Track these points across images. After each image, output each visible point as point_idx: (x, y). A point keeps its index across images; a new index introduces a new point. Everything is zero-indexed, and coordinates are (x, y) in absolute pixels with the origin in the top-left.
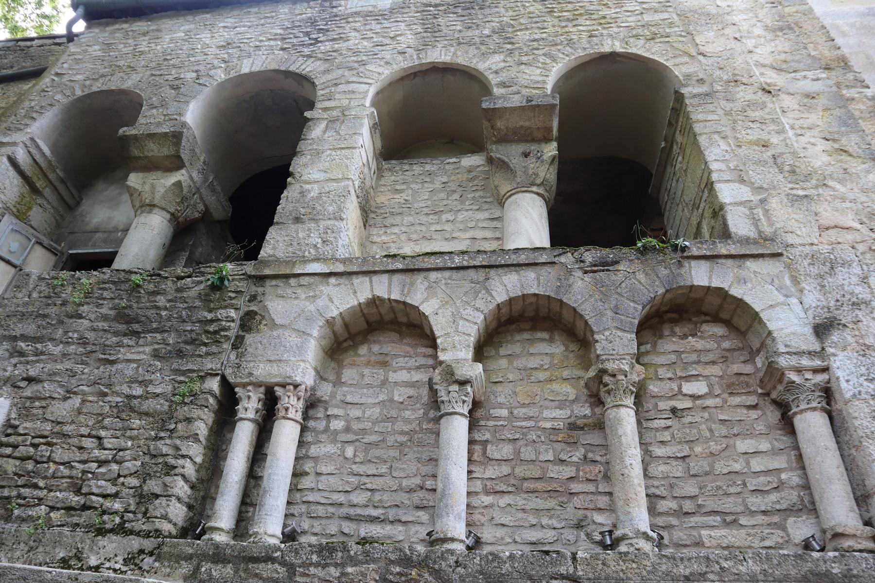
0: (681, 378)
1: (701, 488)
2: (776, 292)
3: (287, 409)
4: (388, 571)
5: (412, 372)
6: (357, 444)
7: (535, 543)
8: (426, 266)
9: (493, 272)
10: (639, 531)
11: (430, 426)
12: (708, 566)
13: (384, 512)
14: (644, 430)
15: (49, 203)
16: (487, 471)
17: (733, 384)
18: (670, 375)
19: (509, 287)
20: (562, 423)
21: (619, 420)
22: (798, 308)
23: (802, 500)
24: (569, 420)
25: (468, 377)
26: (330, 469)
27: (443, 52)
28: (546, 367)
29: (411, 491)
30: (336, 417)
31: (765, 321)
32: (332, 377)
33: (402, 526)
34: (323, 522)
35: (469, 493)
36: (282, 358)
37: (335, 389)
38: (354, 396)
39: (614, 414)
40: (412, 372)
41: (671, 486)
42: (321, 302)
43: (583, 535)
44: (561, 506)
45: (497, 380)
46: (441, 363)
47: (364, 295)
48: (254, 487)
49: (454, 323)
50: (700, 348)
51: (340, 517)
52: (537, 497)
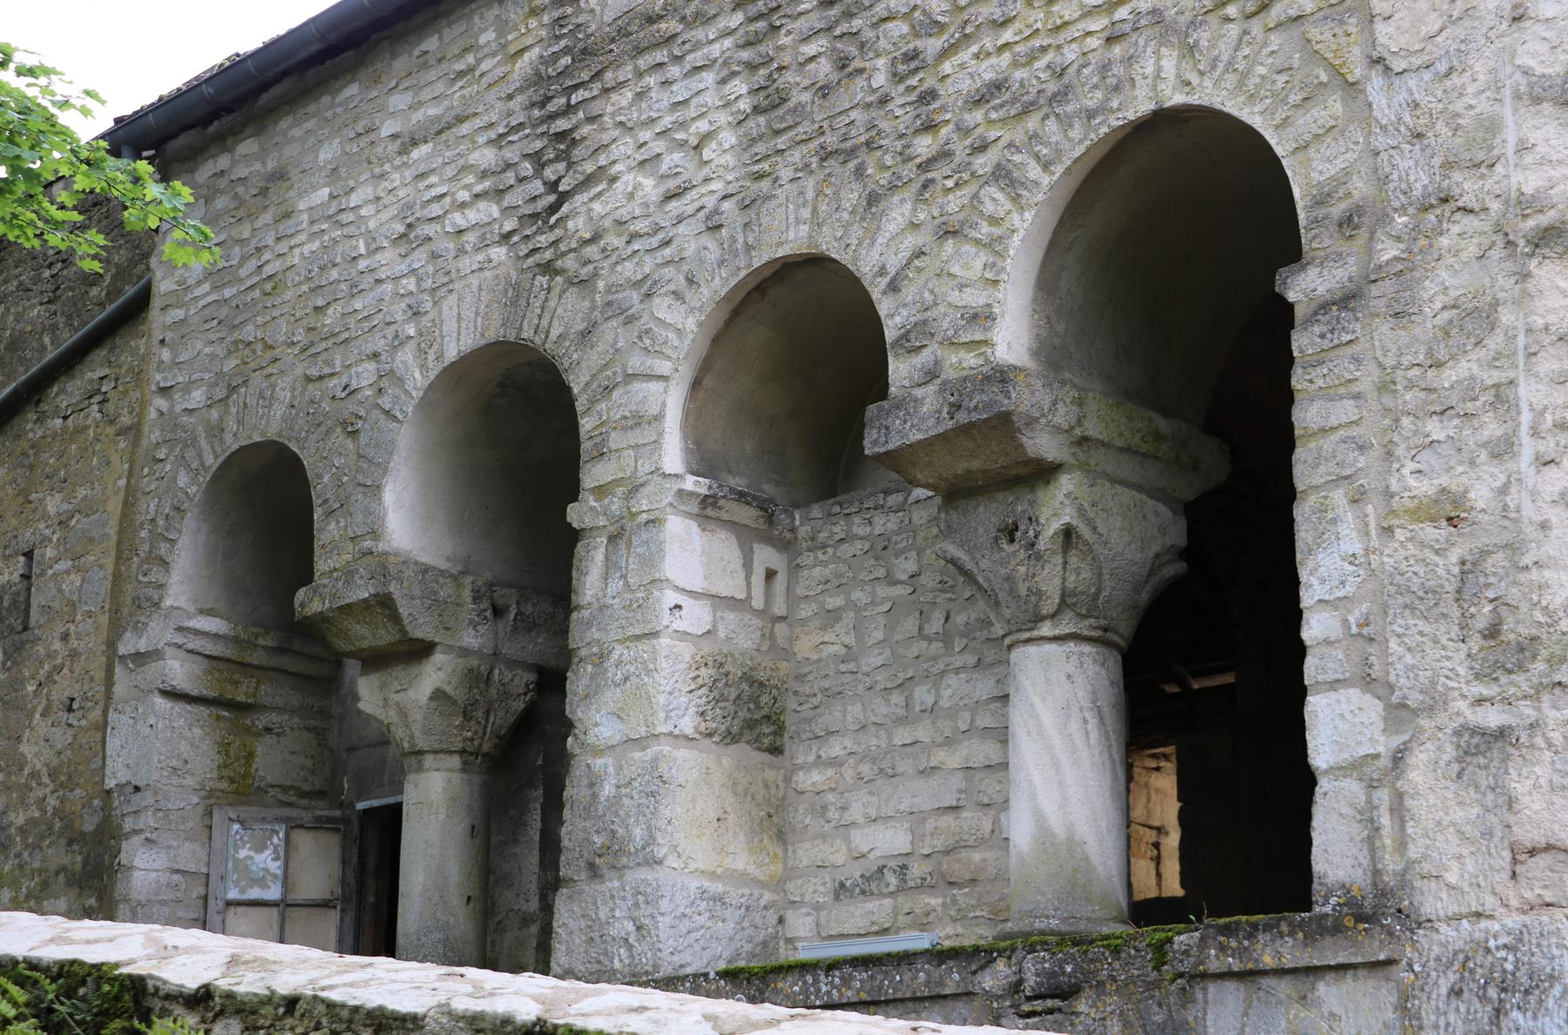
15: (279, 710)
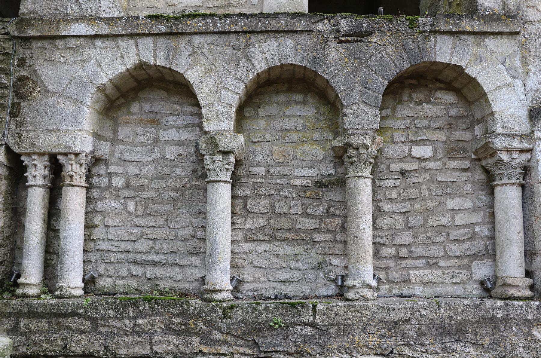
0: (412, 142)
1: (415, 238)
2: (505, 73)
3: (71, 177)
4: (171, 322)
5: (181, 131)
6: (137, 199)
7: (284, 282)
8: (189, 29)
9: (253, 38)
10: (364, 283)
11: (199, 183)
12: (411, 314)
13: (164, 258)
14: (377, 189)
16: (247, 223)
17: (453, 149)
18: (403, 139)
19: (269, 54)
20: (310, 181)
21: (358, 189)
22: (520, 90)
23: (487, 248)
24: (316, 178)
25: (231, 149)
26: (116, 222)
28: (299, 128)
29: (185, 240)
30: (117, 174)
31: (491, 102)
32: (108, 134)
33: (180, 269)
34: (116, 266)
35: (232, 242)
36: (60, 128)
37: (113, 147)
38: (130, 155)
39: (354, 183)
40: (181, 131)
41: (393, 236)
42: (91, 67)
43: (321, 274)
44: (306, 252)
45: (256, 140)
46: (206, 133)
47: (131, 62)
48: (54, 238)
49: (217, 92)
50: (431, 115)
51: (128, 262)
52: (287, 245)
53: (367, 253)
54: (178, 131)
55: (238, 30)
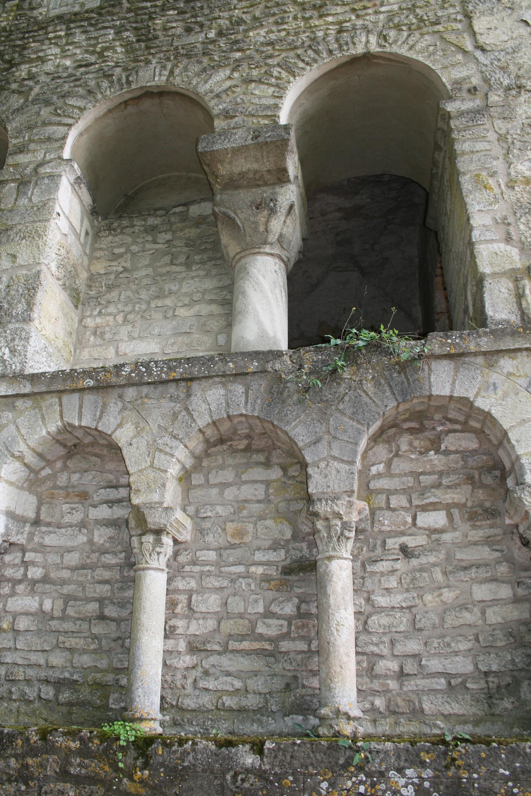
25: (162, 526)
27: (157, 70)
30: (33, 563)
31: (514, 442)
41: (392, 643)
45: (205, 515)
53: (343, 666)
54: (110, 507)
55: (177, 378)
